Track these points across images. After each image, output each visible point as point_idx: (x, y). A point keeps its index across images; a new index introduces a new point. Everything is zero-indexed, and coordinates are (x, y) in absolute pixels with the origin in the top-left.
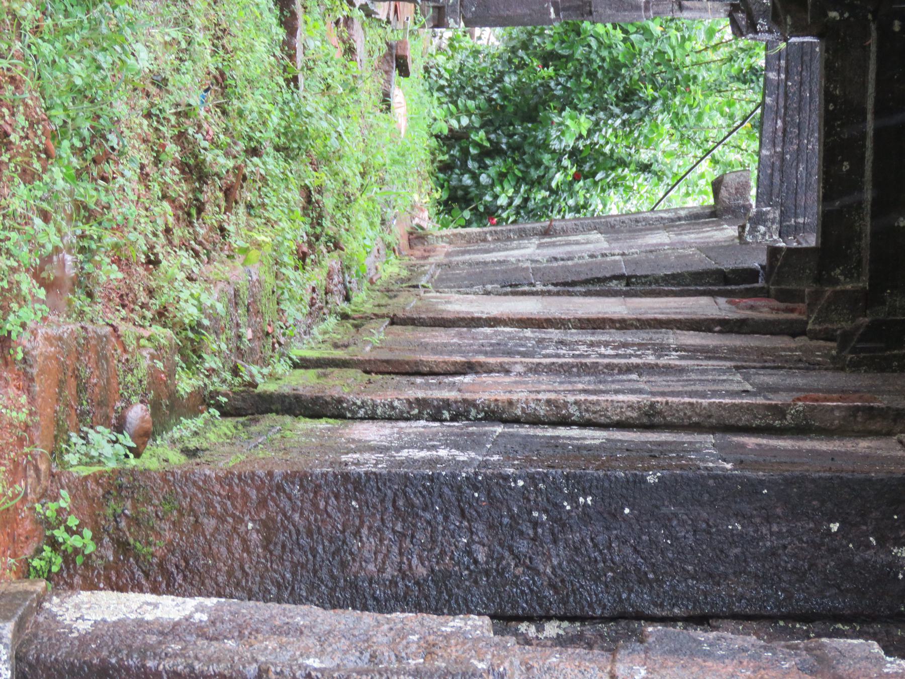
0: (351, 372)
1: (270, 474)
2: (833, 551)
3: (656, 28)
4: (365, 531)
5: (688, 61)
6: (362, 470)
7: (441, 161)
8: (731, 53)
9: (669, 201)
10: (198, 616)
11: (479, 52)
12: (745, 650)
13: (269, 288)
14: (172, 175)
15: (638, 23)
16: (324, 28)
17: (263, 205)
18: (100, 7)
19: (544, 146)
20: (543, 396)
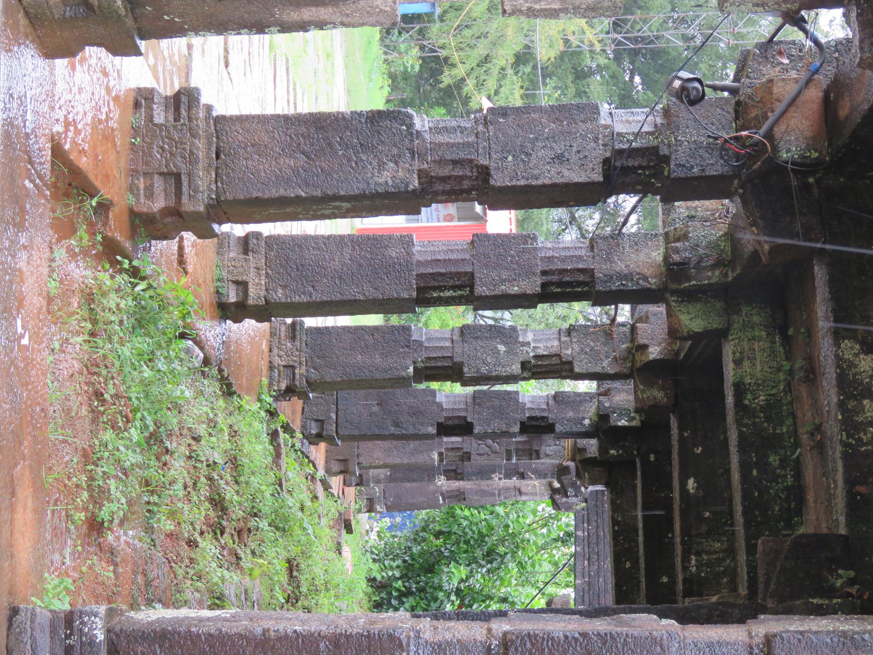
7: (375, 601)
19: (440, 588)
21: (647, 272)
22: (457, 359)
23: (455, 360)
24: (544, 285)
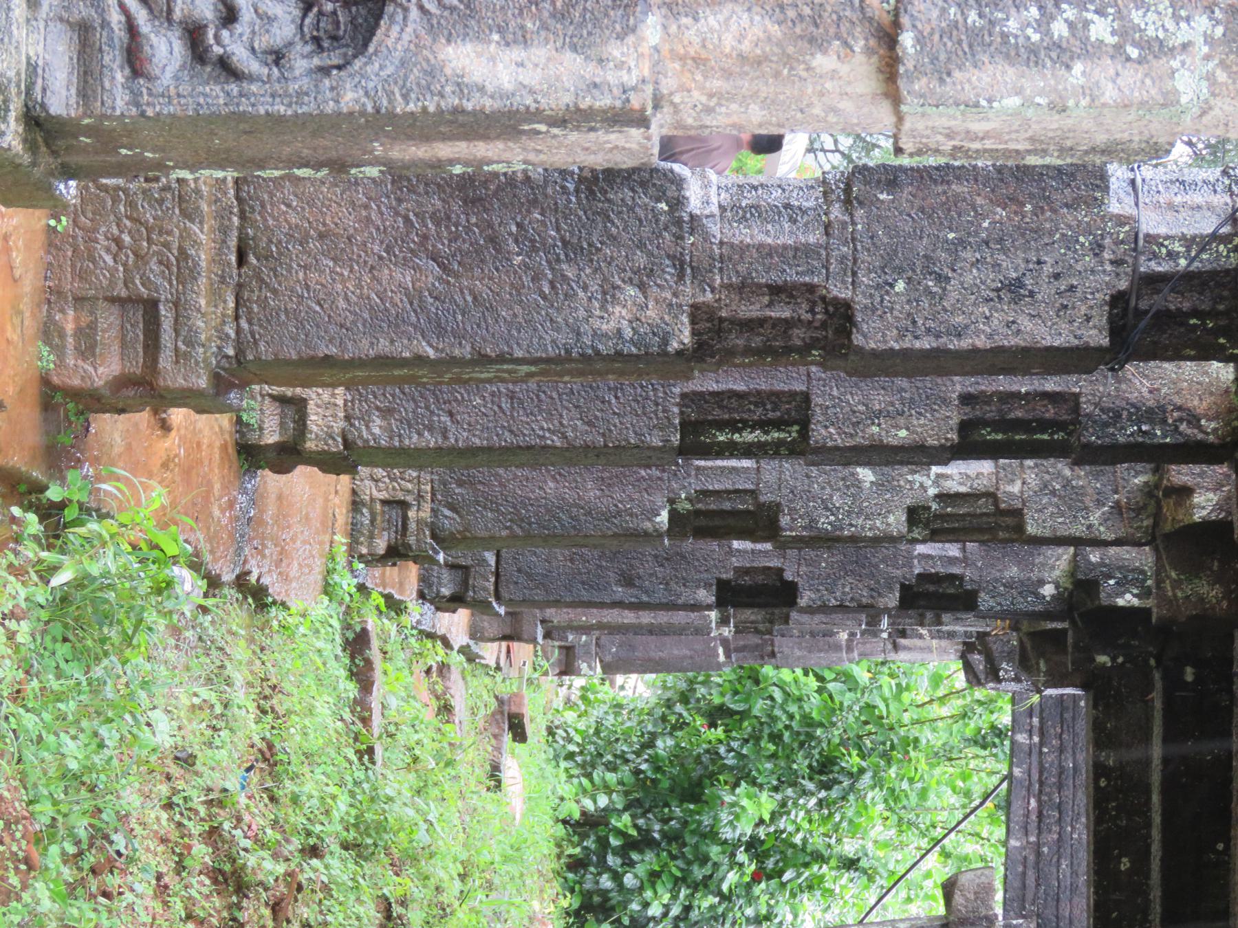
3: (861, 673)
5: (906, 718)
7: (570, 856)
8: (965, 706)
9: (885, 909)
11: (619, 706)
14: (200, 886)
15: (839, 668)
16: (410, 679)
18: (105, 662)
19: (712, 835)
21: (1198, 404)
23: (762, 499)
24: (964, 427)
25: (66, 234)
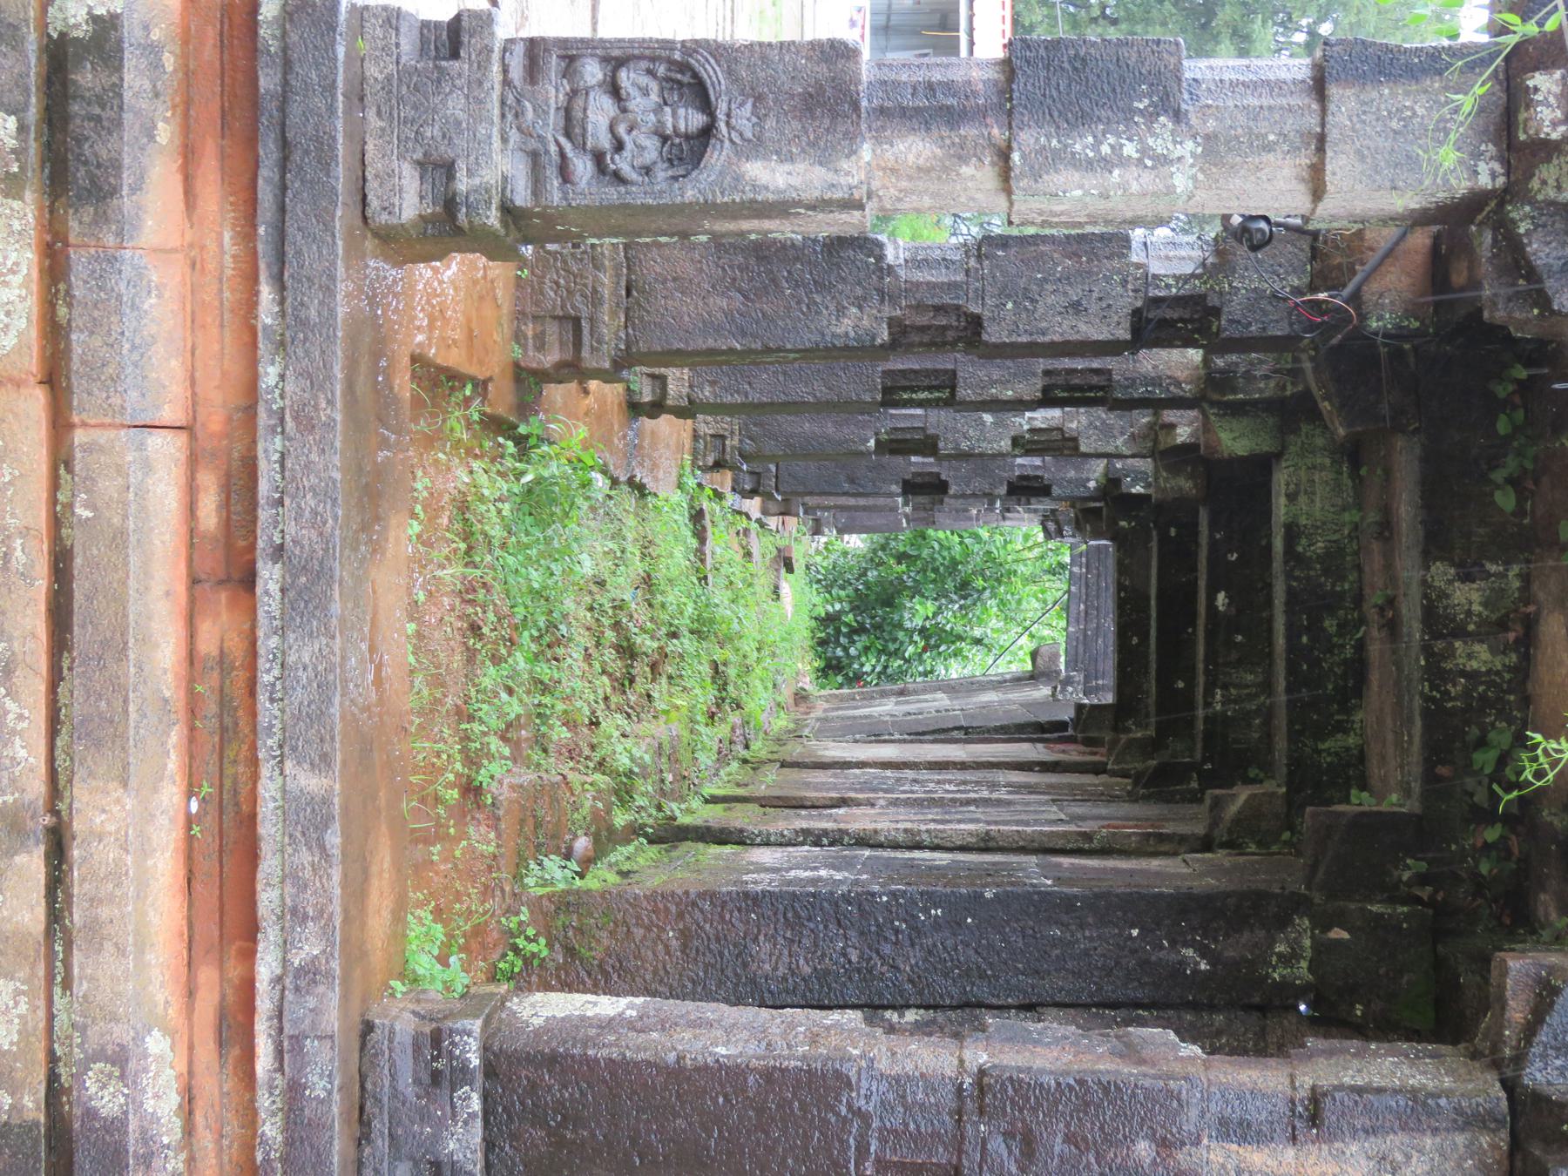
0: (750, 806)
1: (687, 893)
2: (1134, 952)
3: (984, 534)
4: (761, 938)
6: (759, 888)
10: (629, 1013)
12: (1067, 1038)
13: (685, 741)
14: (609, 655)
17: (681, 676)
19: (900, 626)
20: (901, 826)
22: (931, 431)
24: (1046, 390)
25: (527, 279)
